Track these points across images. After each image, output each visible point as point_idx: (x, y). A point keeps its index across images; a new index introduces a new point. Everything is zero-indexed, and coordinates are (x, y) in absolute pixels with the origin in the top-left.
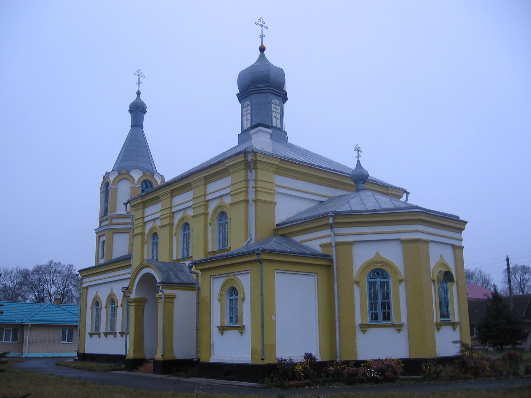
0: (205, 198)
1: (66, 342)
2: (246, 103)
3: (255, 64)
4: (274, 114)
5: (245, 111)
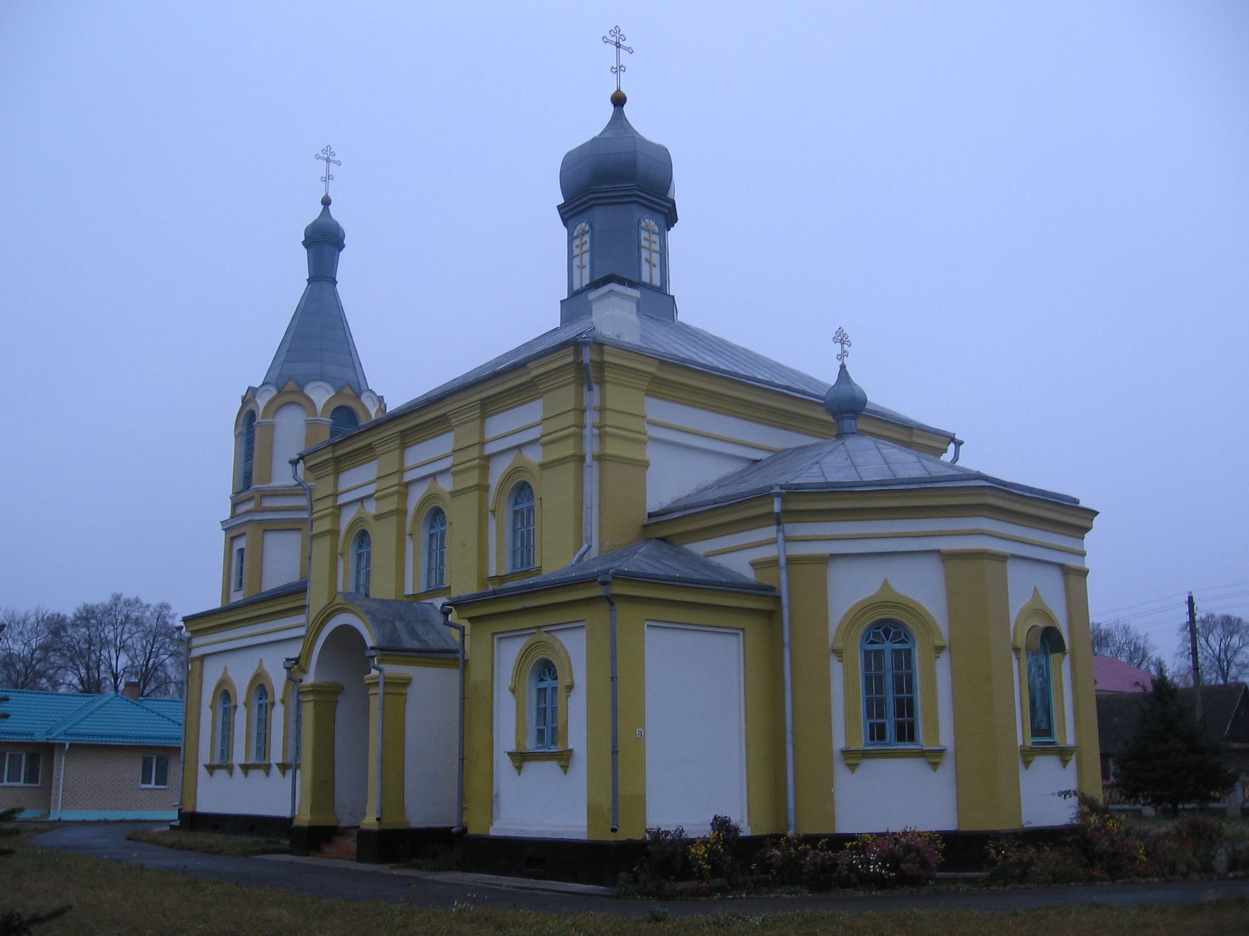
0: (482, 450)
1: (152, 785)
2: (578, 227)
3: (600, 135)
4: (645, 254)
5: (577, 247)
